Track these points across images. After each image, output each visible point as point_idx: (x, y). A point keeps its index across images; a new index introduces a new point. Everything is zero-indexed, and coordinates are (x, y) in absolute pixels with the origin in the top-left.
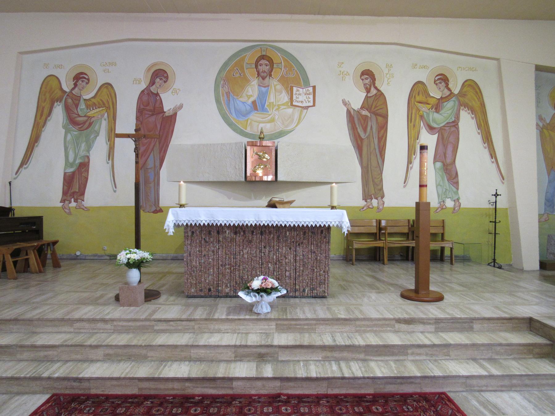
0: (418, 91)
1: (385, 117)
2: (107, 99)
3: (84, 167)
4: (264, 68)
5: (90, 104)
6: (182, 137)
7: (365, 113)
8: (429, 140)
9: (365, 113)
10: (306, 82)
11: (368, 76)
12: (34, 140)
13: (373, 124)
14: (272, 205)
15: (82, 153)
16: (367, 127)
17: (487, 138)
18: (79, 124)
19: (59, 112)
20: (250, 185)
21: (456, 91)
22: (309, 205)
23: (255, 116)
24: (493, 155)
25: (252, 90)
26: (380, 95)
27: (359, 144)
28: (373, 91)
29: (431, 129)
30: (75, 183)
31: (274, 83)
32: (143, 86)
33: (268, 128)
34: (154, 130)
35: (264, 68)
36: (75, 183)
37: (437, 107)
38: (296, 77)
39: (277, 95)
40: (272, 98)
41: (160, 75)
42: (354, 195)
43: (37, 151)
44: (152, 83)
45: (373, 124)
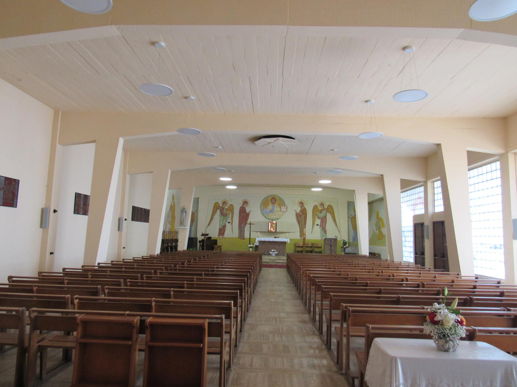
0: (315, 207)
1: (306, 215)
2: (231, 208)
3: (225, 226)
4: (273, 201)
5: (227, 210)
6: (250, 220)
7: (301, 213)
8: (318, 221)
9: (301, 213)
10: (285, 205)
11: (301, 203)
12: (212, 219)
13: (303, 216)
14: (275, 238)
15: (224, 223)
16: (301, 217)
17: (335, 221)
18: (223, 215)
19: (218, 212)
20: (269, 233)
21: (326, 208)
22: (404, 92)
23: (271, 214)
24: (336, 225)
25: (270, 207)
26: (305, 209)
27: (299, 222)
28: (303, 208)
29: (319, 218)
30: (222, 231)
31: (276, 205)
32: (241, 205)
33: (274, 217)
34: (244, 216)
35: (273, 201)
36: (222, 231)
37: (321, 212)
38: (282, 203)
39: (277, 208)
40: (275, 209)
41: (245, 203)
42: (297, 236)
43: (212, 222)
44: (244, 204)
45: (303, 216)
